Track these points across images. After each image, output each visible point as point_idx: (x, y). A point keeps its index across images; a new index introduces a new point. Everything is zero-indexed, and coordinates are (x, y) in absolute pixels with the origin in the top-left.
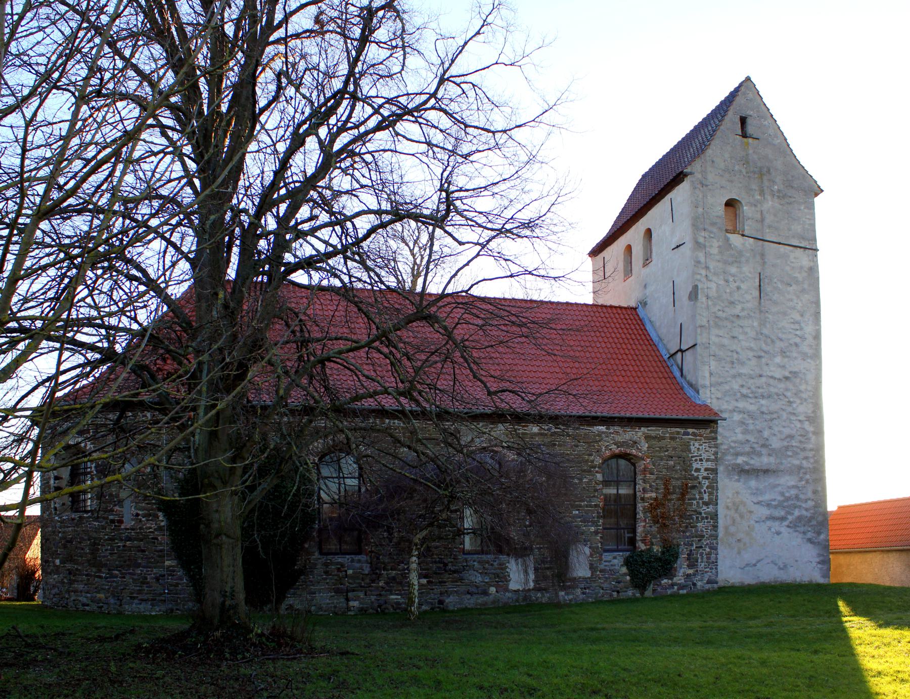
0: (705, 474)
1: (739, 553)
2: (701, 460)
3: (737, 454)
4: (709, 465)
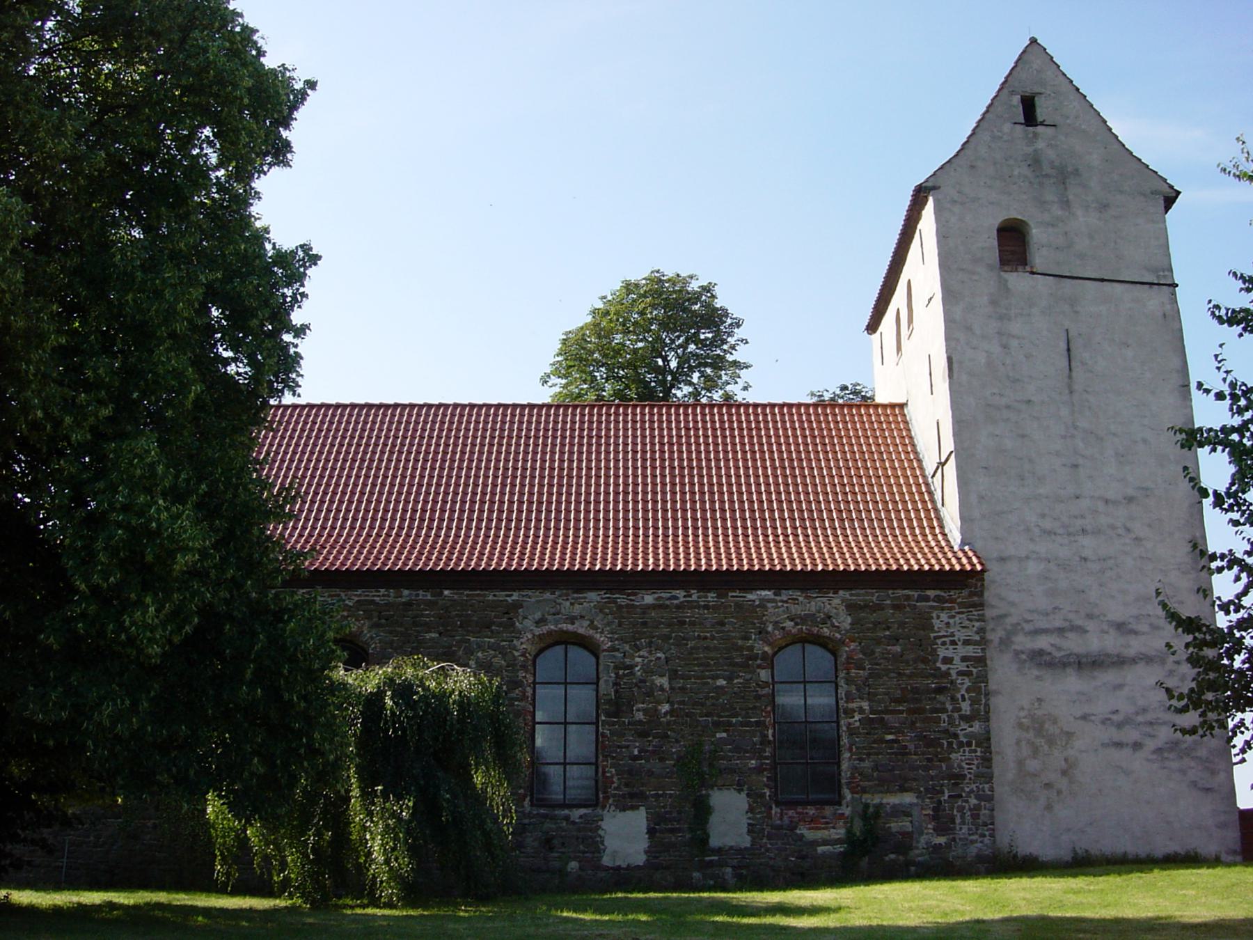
0: (962, 667)
1: (1049, 807)
2: (954, 643)
3: (1037, 632)
4: (970, 651)
